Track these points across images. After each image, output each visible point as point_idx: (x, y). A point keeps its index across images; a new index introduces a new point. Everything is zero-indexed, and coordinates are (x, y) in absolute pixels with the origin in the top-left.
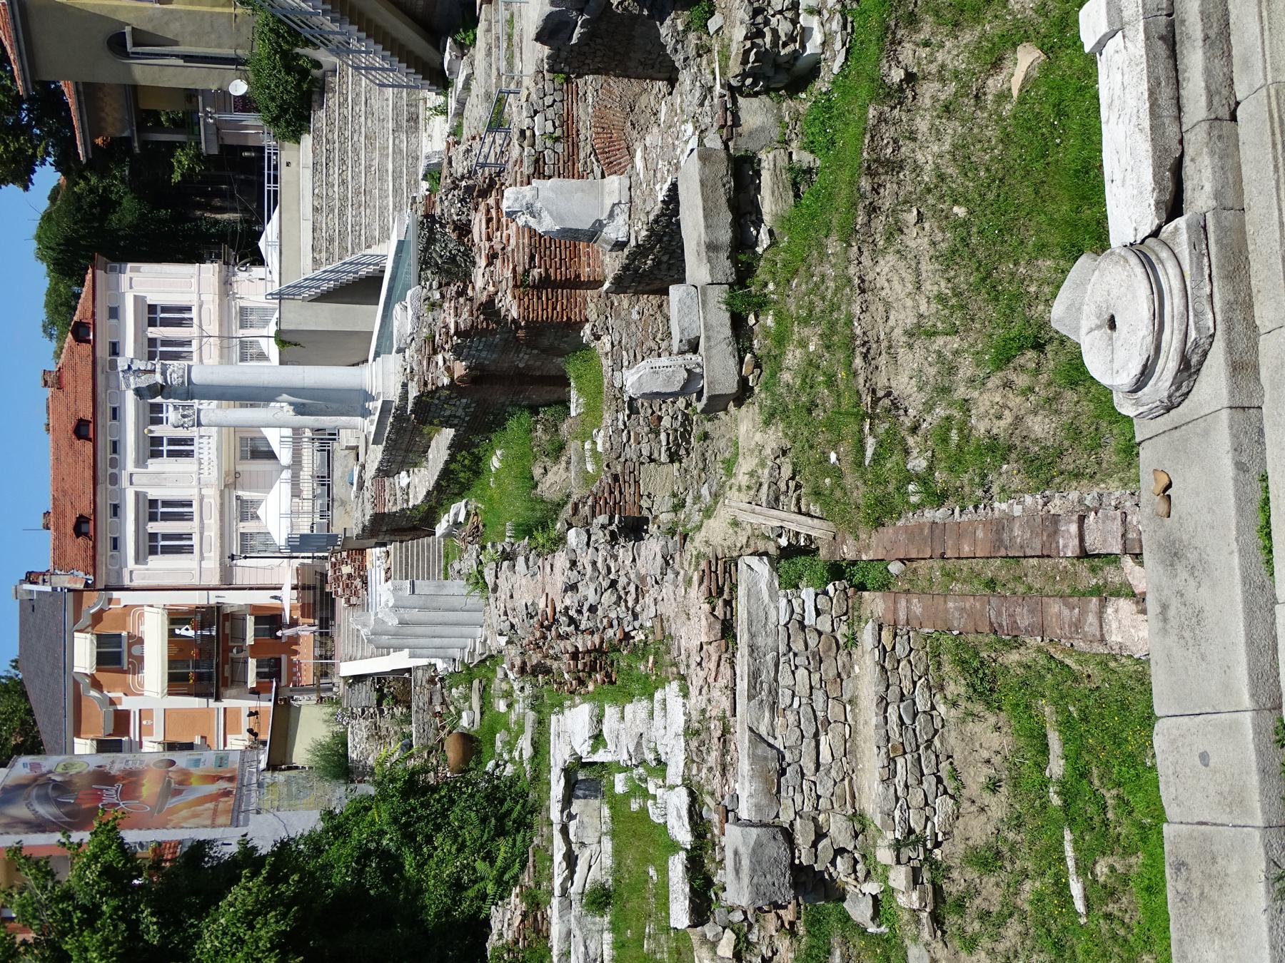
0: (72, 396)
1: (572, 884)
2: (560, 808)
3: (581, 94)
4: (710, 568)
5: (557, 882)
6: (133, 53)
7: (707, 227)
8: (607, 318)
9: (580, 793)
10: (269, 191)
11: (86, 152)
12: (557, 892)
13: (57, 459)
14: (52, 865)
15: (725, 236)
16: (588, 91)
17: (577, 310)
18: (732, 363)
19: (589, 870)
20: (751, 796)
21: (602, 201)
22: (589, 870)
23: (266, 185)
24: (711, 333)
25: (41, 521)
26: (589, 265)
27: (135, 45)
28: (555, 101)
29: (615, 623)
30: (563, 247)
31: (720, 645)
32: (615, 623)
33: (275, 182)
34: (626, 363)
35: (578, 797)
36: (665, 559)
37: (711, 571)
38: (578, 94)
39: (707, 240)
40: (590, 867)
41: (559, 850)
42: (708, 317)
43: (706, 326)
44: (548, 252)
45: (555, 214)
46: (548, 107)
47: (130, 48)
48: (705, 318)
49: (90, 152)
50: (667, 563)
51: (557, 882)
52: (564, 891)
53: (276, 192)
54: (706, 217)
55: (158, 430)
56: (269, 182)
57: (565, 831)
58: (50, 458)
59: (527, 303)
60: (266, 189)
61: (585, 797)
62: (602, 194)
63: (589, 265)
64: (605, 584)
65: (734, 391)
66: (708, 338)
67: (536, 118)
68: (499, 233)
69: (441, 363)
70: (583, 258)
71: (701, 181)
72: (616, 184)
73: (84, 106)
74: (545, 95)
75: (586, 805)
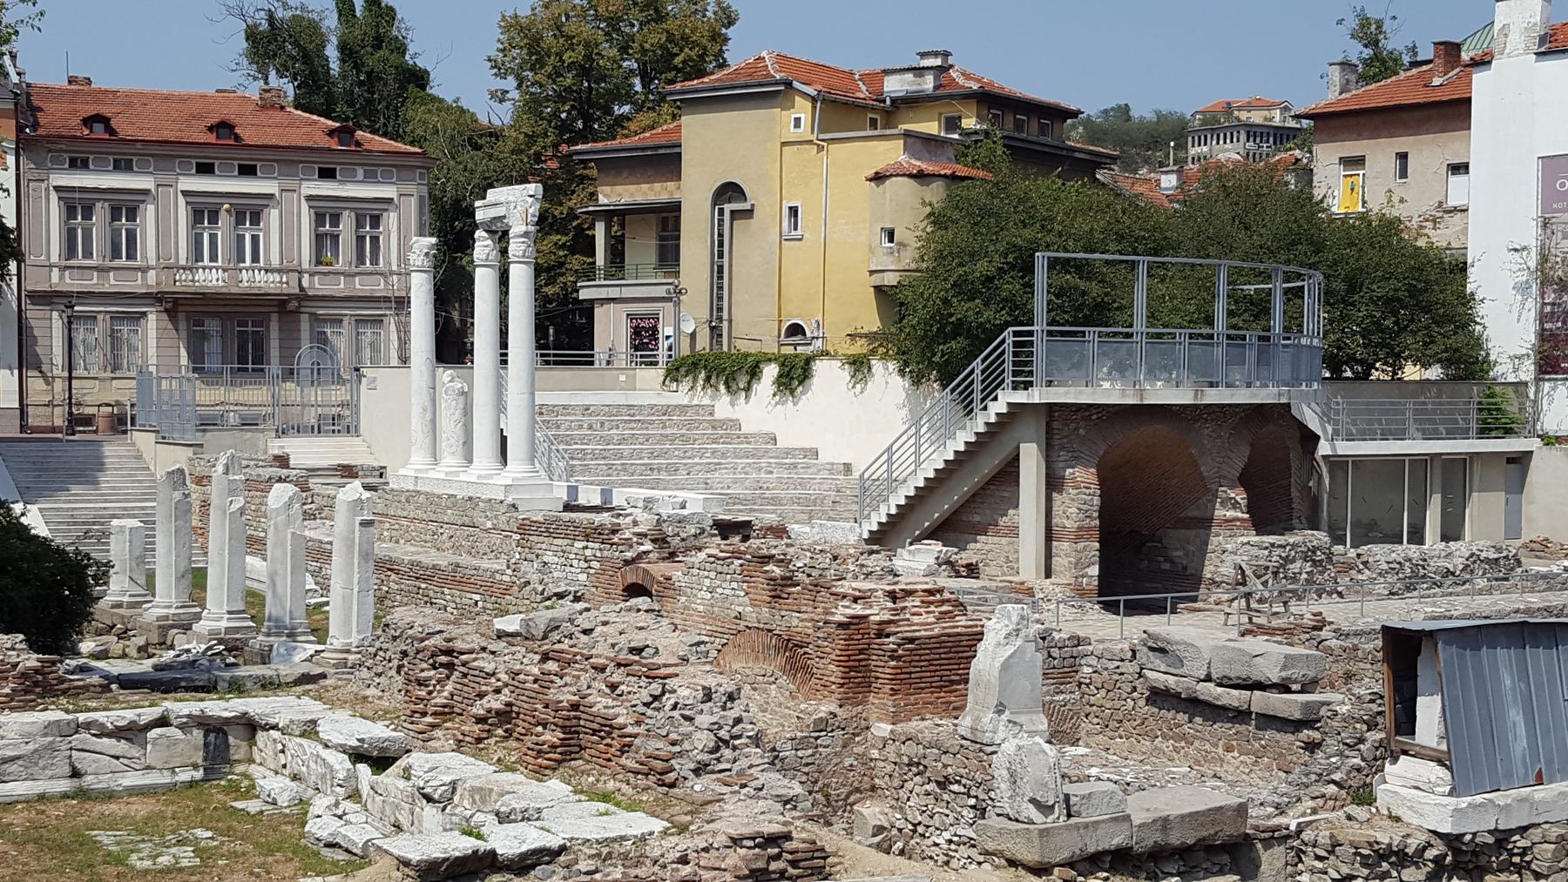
0: (255, 121)
1: (94, 735)
2: (194, 713)
3: (1062, 687)
4: (817, 850)
5: (100, 716)
6: (721, 212)
7: (1183, 817)
8: (843, 729)
9: (212, 736)
12: (82, 717)
13: (167, 98)
15: (1175, 839)
16: (1064, 696)
17: (851, 695)
18: (1064, 855)
19: (112, 756)
21: (1023, 713)
22: (112, 756)
25: (81, 74)
26: (906, 705)
27: (732, 212)
28: (1055, 659)
29: (677, 749)
31: (741, 868)
32: (677, 749)
35: (206, 736)
36: (791, 799)
38: (1062, 684)
39: (1171, 818)
40: (117, 758)
41: (139, 715)
43: (1097, 822)
44: (917, 658)
45: (1012, 660)
46: (1049, 652)
47: (728, 207)
48: (1103, 821)
50: (786, 803)
51: (100, 716)
52: (78, 727)
54: (1191, 815)
55: (225, 220)
56: (641, 356)
57: (163, 722)
58: (165, 90)
59: (856, 637)
61: (206, 745)
62: (1030, 712)
63: (906, 705)
64: (723, 734)
66: (1086, 826)
68: (919, 604)
69: (642, 548)
70: (912, 698)
71: (1221, 808)
73: (1087, 157)
74: (1060, 648)
75: (196, 748)
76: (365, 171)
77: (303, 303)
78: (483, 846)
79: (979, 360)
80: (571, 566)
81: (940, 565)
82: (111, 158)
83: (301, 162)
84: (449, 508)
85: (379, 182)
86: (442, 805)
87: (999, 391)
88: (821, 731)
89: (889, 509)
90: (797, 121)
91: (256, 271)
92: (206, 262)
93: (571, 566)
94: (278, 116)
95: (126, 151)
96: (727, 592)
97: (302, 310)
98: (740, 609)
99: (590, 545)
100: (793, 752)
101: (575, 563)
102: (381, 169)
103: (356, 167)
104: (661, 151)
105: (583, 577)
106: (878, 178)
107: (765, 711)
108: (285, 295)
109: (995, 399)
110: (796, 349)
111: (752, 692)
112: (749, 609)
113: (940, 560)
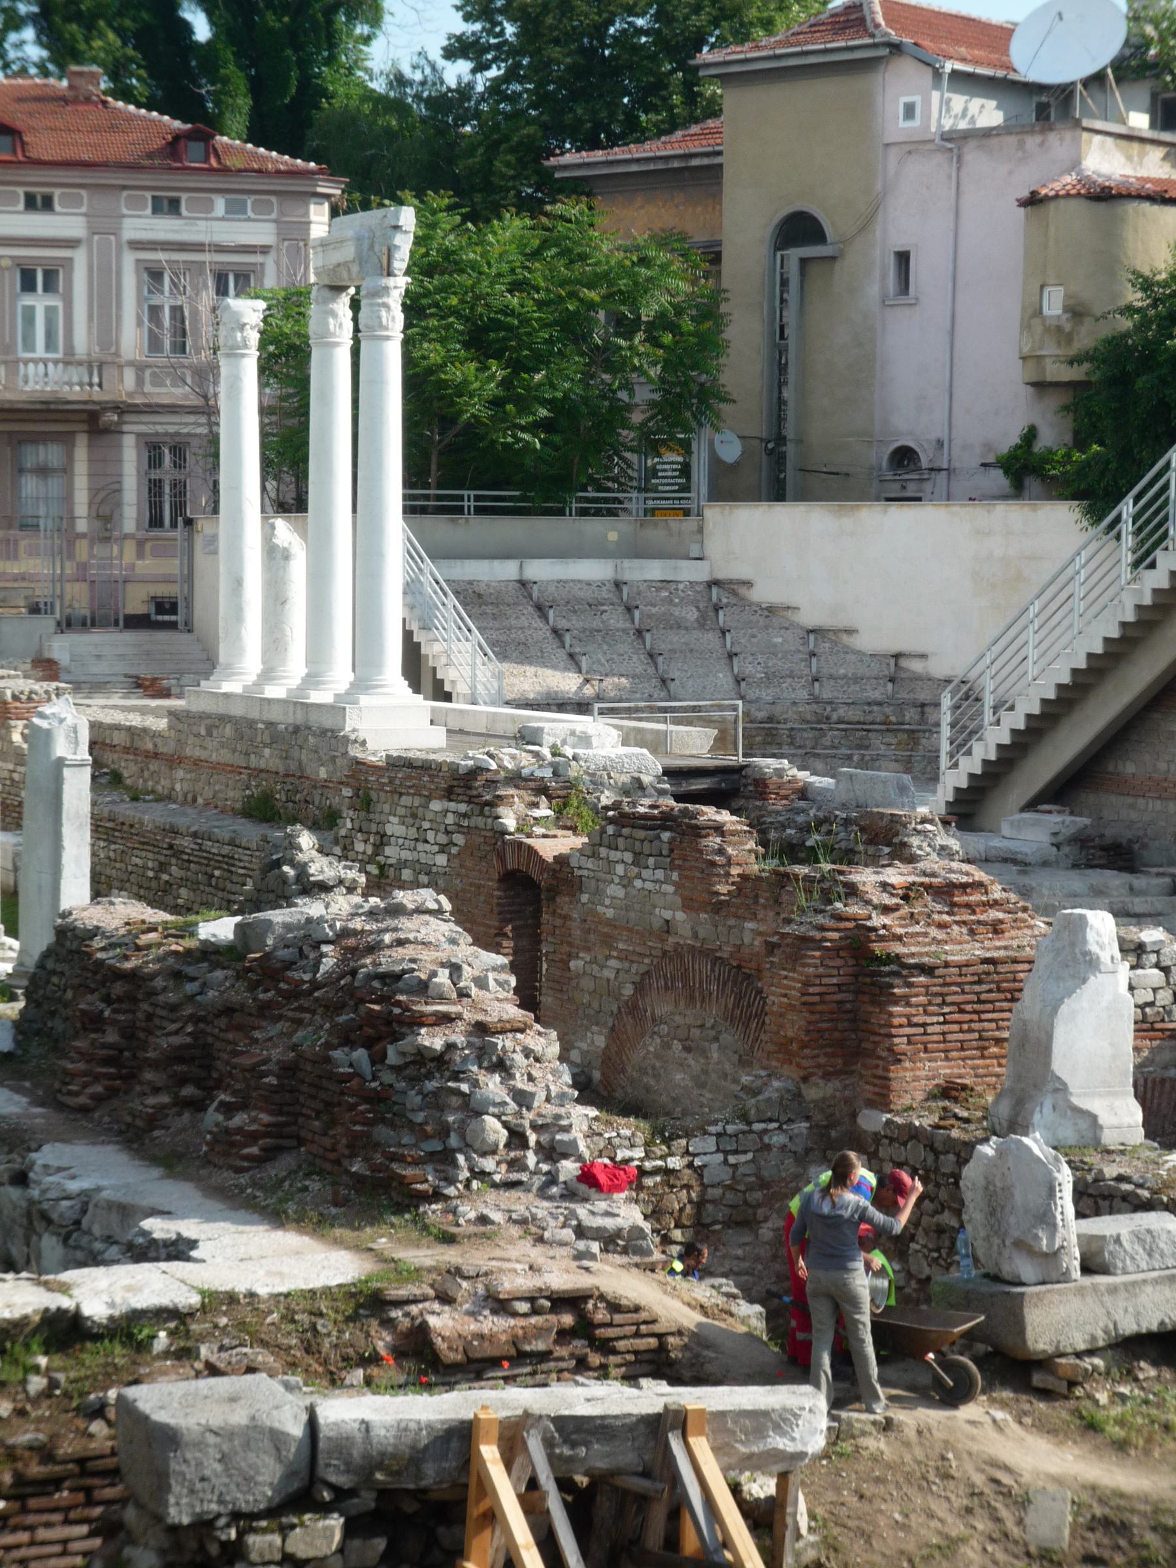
10: (461, 498)
11: (566, 167)
14: (1134, 40)
20: (366, 1426)
23: (472, 493)
24: (1123, 1294)
27: (804, 262)
30: (946, 1028)
33: (480, 511)
34: (732, 1159)
37: (638, 1324)
42: (1149, 1289)
43: (1134, 1284)
47: (795, 254)
48: (1145, 1281)
49: (567, 174)
53: (459, 510)
56: (478, 498)
60: (465, 493)
62: (1109, 1094)
65: (1030, 1344)
66: (1113, 1290)
67: (1156, 971)
72: (1127, 1120)
76: (228, 202)
77: (127, 417)
78: (66, 1303)
79: (1129, 500)
80: (426, 841)
81: (1058, 846)
82: (148, 195)
83: (124, 187)
84: (265, 745)
85: (249, 220)
86: (63, 1231)
87: (1158, 553)
88: (771, 1120)
89: (986, 752)
90: (910, 111)
91: (51, 366)
92: (40, 351)
93: (426, 841)
94: (94, 115)
95: (9, 178)
96: (649, 885)
97: (126, 428)
98: (667, 914)
99: (452, 806)
100: (720, 1157)
101: (430, 836)
102: (253, 197)
103: (213, 196)
104: (695, 162)
105: (441, 860)
106: (1033, 201)
107: (702, 1086)
108: (94, 402)
109: (1152, 566)
110: (904, 488)
111: (684, 1055)
112: (680, 916)
113: (1060, 838)
